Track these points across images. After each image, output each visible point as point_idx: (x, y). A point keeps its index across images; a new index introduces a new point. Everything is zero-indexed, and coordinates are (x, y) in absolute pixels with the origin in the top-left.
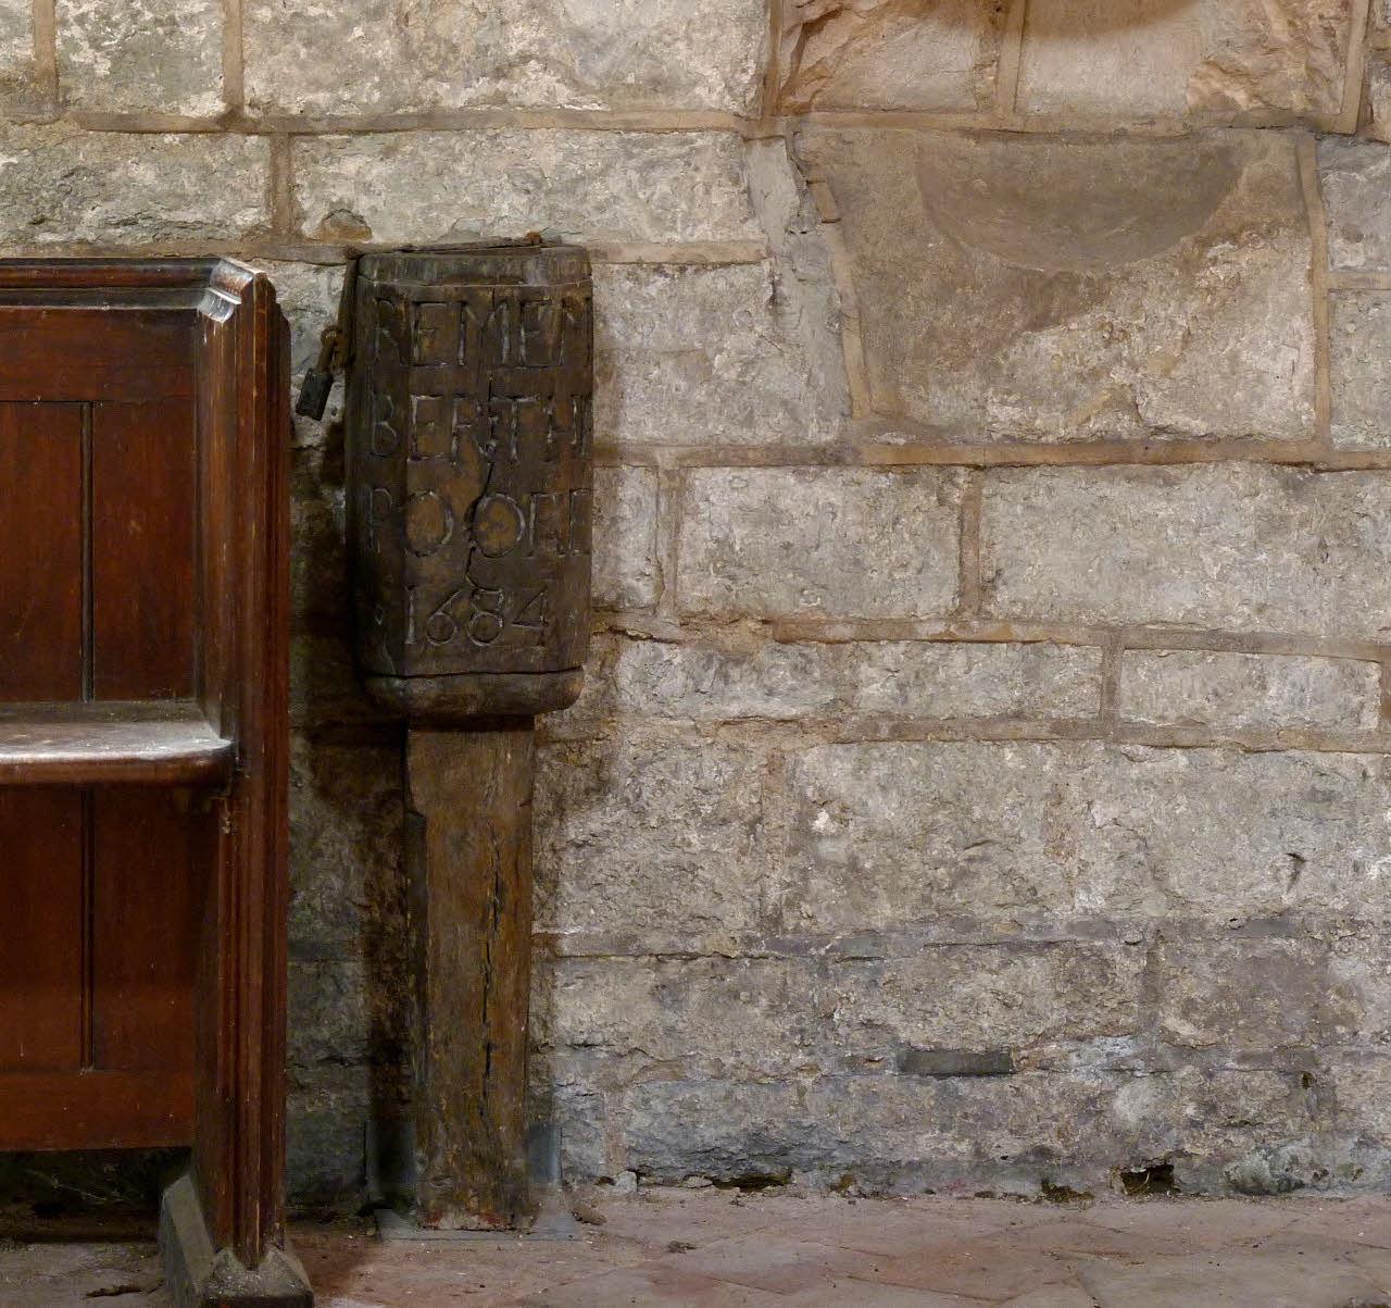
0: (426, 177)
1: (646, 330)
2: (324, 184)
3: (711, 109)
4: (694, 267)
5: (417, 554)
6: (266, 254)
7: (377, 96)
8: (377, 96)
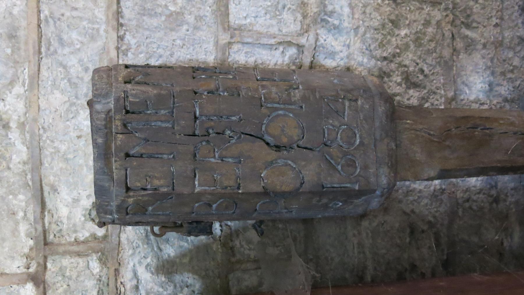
0: (69, 168)
1: (155, 46)
2: (74, 225)
3: (26, 4)
4: (120, 19)
5: (302, 184)
6: (116, 255)
7: (21, 197)
8: (21, 197)
